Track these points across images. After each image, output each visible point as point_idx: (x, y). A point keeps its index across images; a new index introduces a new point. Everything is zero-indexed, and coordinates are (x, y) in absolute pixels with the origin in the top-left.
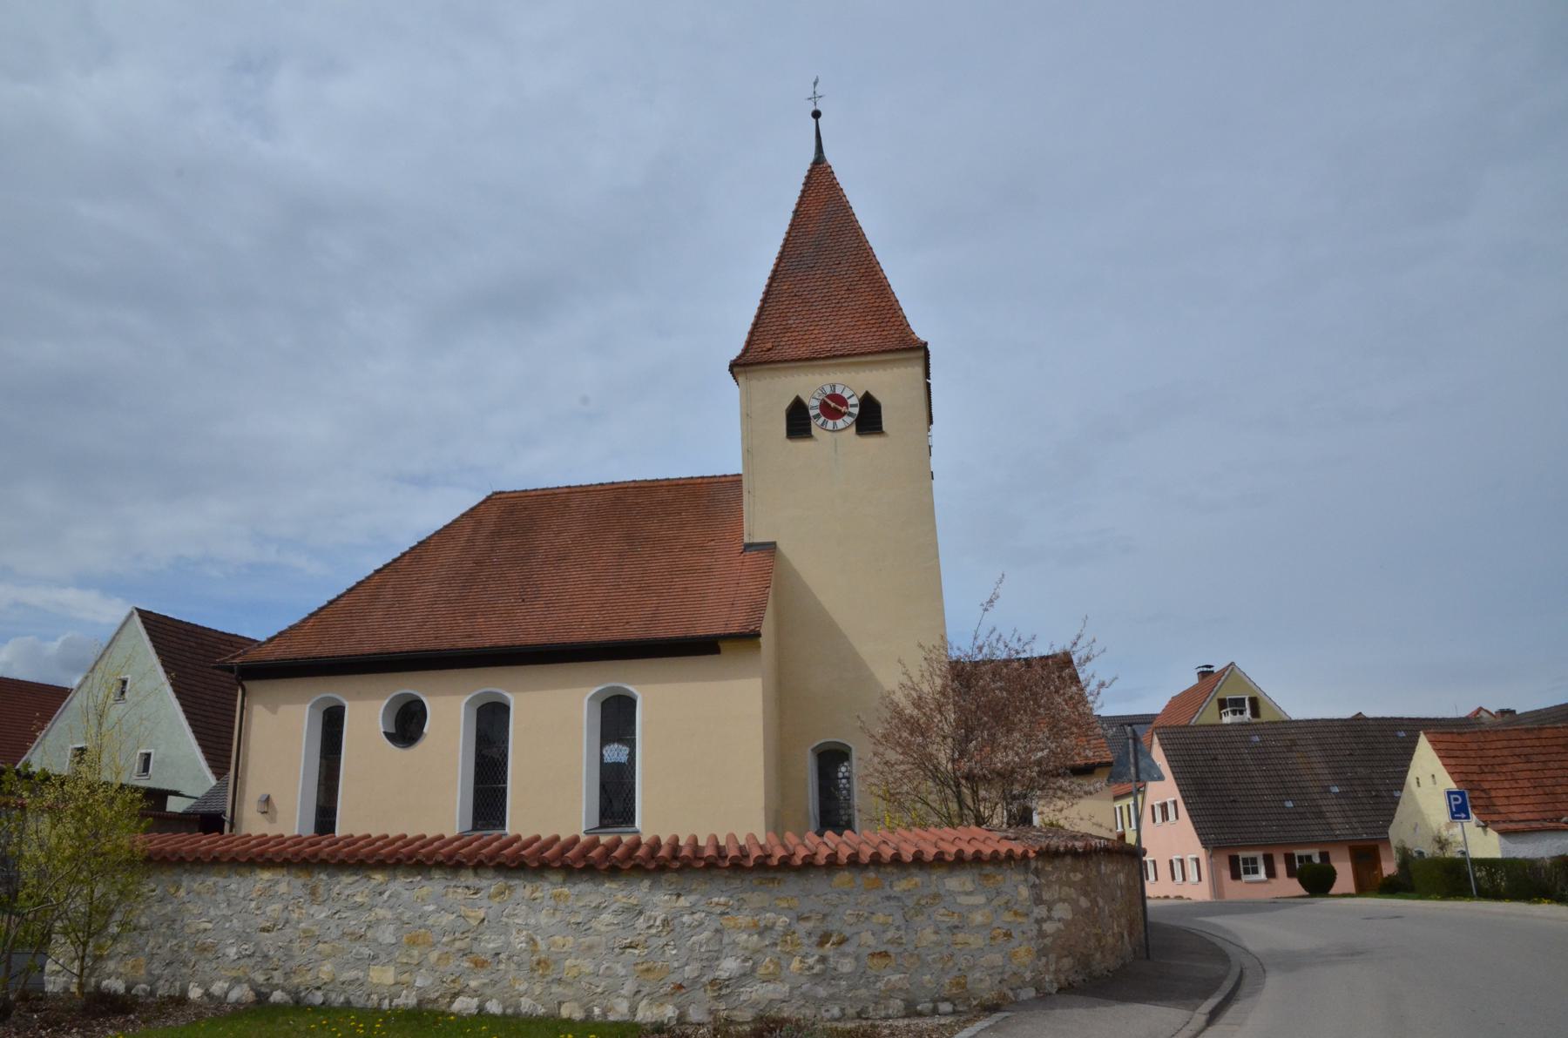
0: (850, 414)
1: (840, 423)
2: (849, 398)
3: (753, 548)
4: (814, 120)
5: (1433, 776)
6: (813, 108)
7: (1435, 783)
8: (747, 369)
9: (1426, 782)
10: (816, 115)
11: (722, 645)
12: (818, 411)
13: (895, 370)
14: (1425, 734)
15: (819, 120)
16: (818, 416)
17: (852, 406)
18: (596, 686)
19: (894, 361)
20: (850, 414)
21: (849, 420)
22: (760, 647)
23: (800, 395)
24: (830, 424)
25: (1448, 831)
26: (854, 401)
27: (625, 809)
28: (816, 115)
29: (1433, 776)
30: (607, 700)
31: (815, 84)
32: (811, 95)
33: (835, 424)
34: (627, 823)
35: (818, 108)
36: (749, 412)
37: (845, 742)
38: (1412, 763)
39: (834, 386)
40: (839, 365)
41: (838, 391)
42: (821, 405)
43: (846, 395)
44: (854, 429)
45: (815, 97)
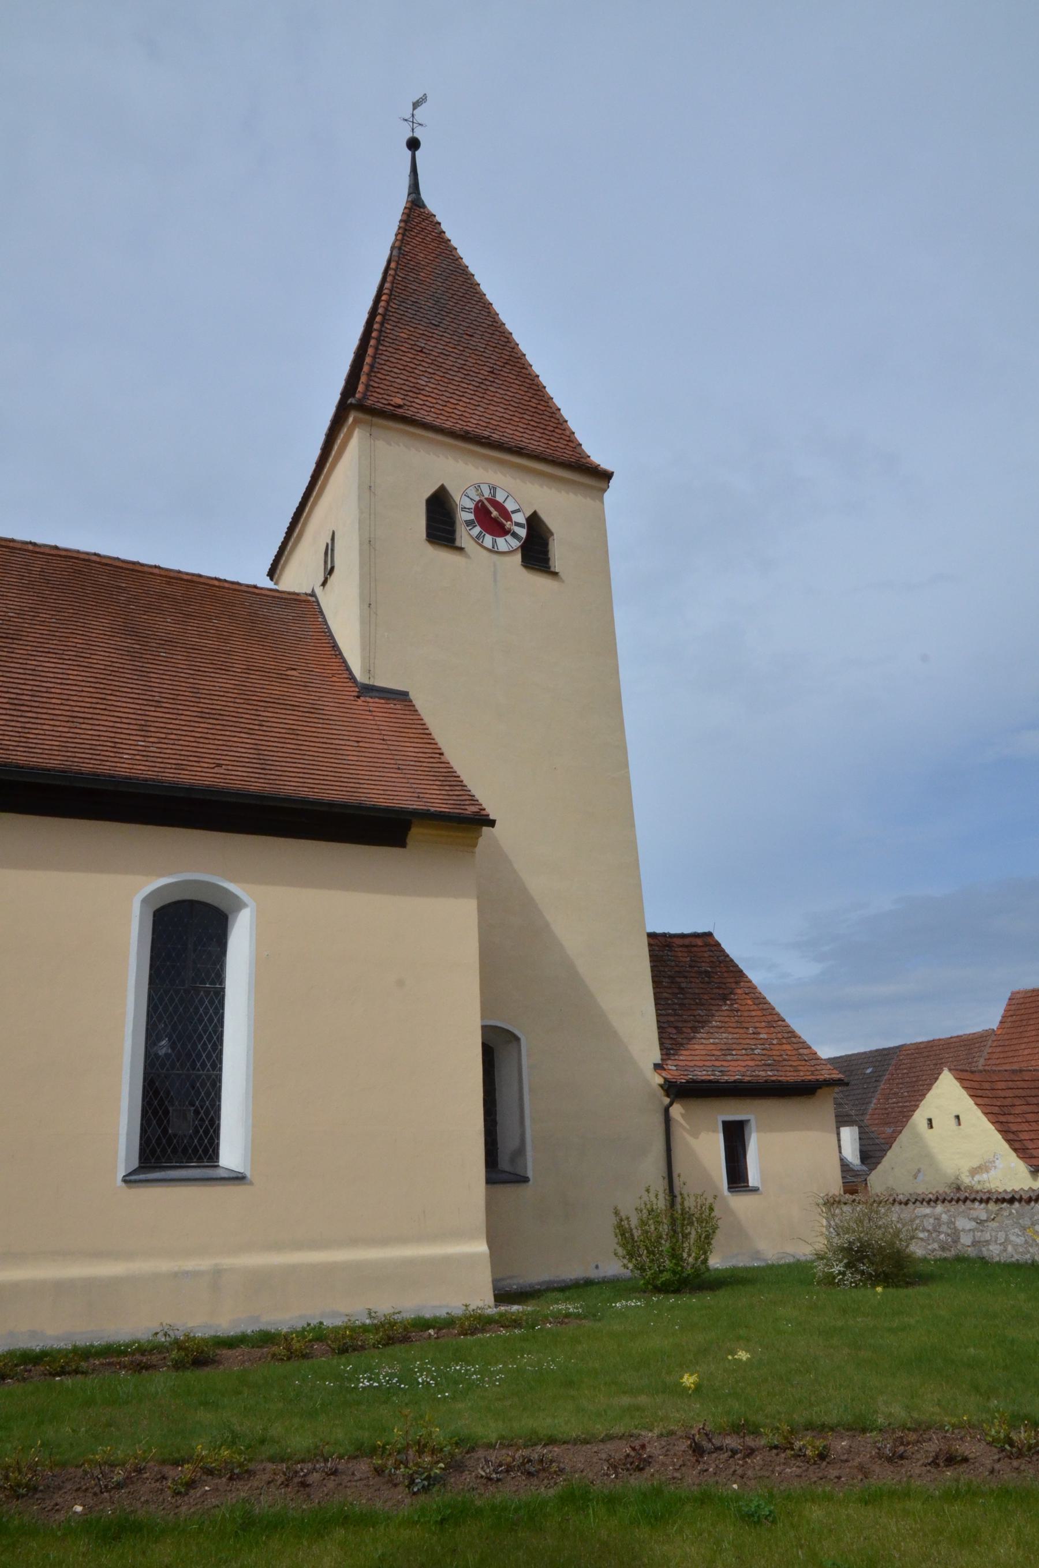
0: (515, 535)
1: (502, 543)
2: (514, 512)
3: (375, 694)
4: (409, 153)
5: (958, 1117)
6: (409, 135)
7: (959, 1124)
8: (375, 420)
9: (944, 1123)
10: (413, 144)
11: (416, 833)
12: (471, 517)
13: (572, 496)
14: (950, 1070)
15: (417, 153)
16: (469, 523)
17: (518, 524)
18: (162, 875)
19: (573, 483)
20: (515, 535)
21: (515, 543)
22: (475, 845)
23: (445, 484)
24: (488, 540)
25: (973, 1177)
26: (520, 518)
27: (196, 1131)
28: (413, 144)
29: (958, 1117)
30: (163, 908)
31: (416, 105)
32: (408, 116)
33: (494, 542)
34: (200, 1159)
35: (416, 135)
36: (372, 485)
37: (511, 1029)
38: (923, 1102)
39: (495, 489)
40: (501, 462)
41: (500, 497)
42: (476, 506)
43: (510, 506)
44: (518, 557)
45: (412, 121)
